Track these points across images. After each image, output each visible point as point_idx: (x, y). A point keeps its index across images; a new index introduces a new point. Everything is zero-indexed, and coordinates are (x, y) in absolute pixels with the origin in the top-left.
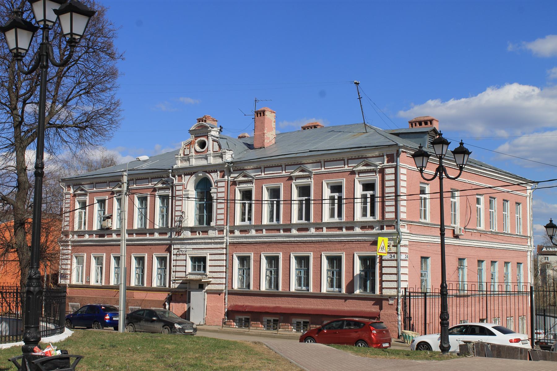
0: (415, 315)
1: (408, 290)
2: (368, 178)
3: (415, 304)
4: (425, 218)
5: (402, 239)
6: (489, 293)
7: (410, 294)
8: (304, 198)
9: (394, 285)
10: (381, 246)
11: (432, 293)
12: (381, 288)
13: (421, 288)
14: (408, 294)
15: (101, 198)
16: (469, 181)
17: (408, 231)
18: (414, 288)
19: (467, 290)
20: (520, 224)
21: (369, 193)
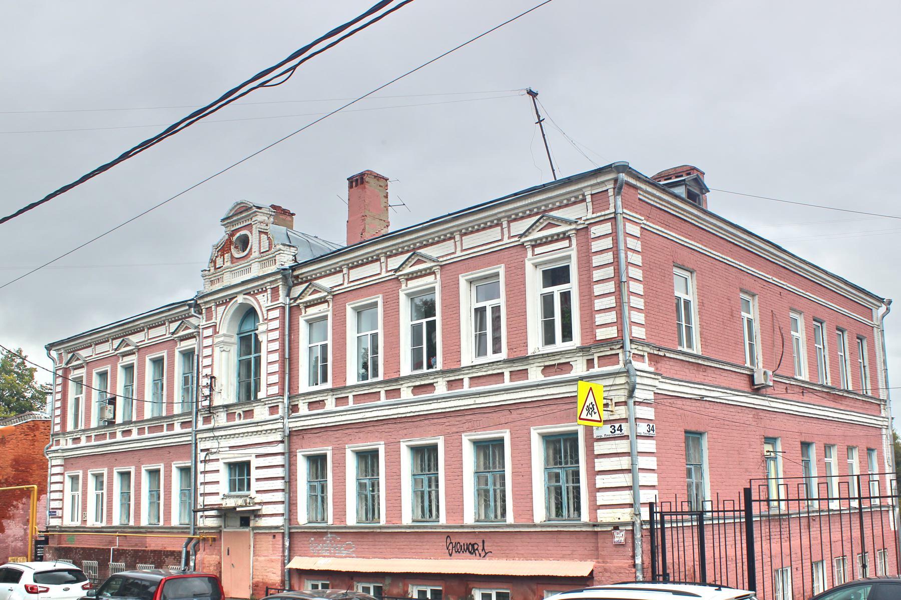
0: (676, 567)
1: (658, 509)
2: (552, 254)
3: (675, 541)
4: (690, 345)
5: (637, 386)
6: (865, 504)
7: (662, 517)
8: (424, 321)
9: (625, 497)
10: (587, 404)
11: (718, 511)
12: (595, 507)
13: (689, 502)
14: (659, 518)
15: (102, 369)
16: (774, 279)
17: (652, 369)
18: (673, 504)
19: (819, 499)
20: (865, 377)
21: (557, 290)
